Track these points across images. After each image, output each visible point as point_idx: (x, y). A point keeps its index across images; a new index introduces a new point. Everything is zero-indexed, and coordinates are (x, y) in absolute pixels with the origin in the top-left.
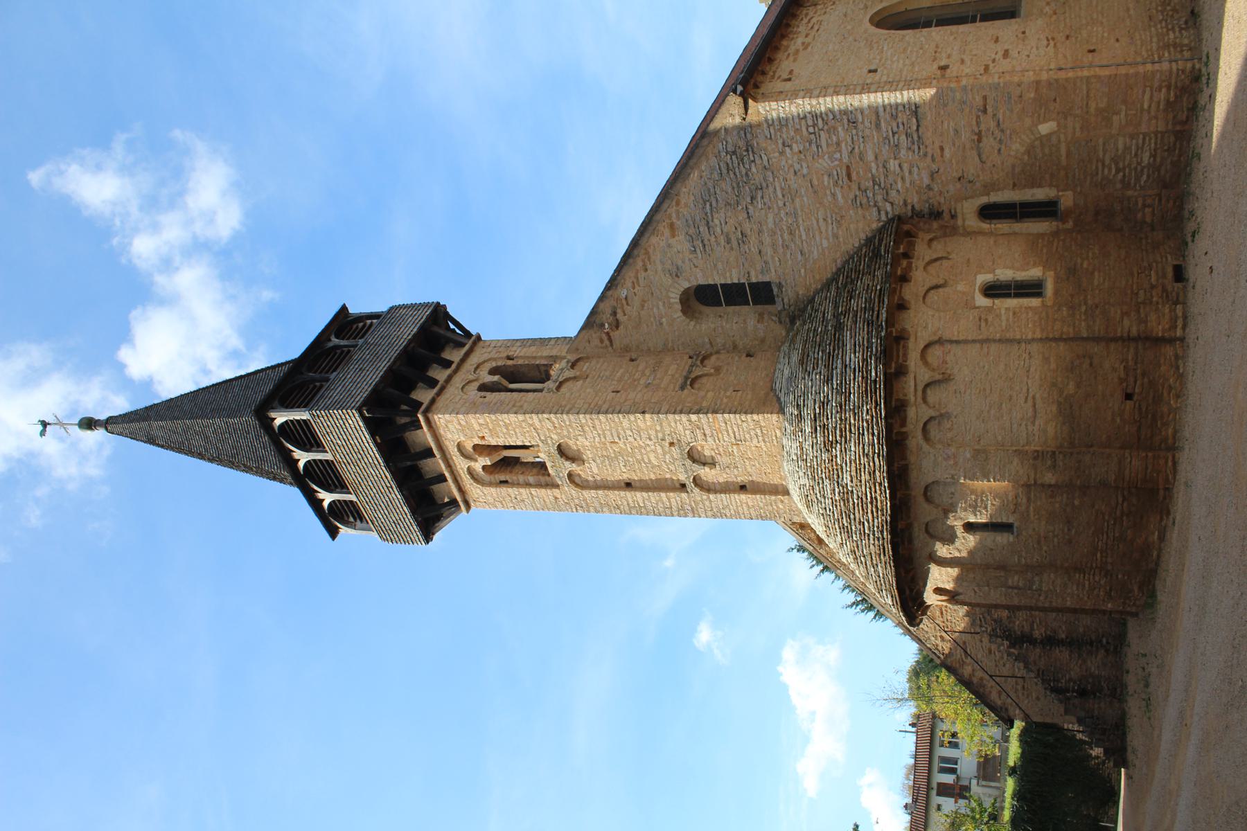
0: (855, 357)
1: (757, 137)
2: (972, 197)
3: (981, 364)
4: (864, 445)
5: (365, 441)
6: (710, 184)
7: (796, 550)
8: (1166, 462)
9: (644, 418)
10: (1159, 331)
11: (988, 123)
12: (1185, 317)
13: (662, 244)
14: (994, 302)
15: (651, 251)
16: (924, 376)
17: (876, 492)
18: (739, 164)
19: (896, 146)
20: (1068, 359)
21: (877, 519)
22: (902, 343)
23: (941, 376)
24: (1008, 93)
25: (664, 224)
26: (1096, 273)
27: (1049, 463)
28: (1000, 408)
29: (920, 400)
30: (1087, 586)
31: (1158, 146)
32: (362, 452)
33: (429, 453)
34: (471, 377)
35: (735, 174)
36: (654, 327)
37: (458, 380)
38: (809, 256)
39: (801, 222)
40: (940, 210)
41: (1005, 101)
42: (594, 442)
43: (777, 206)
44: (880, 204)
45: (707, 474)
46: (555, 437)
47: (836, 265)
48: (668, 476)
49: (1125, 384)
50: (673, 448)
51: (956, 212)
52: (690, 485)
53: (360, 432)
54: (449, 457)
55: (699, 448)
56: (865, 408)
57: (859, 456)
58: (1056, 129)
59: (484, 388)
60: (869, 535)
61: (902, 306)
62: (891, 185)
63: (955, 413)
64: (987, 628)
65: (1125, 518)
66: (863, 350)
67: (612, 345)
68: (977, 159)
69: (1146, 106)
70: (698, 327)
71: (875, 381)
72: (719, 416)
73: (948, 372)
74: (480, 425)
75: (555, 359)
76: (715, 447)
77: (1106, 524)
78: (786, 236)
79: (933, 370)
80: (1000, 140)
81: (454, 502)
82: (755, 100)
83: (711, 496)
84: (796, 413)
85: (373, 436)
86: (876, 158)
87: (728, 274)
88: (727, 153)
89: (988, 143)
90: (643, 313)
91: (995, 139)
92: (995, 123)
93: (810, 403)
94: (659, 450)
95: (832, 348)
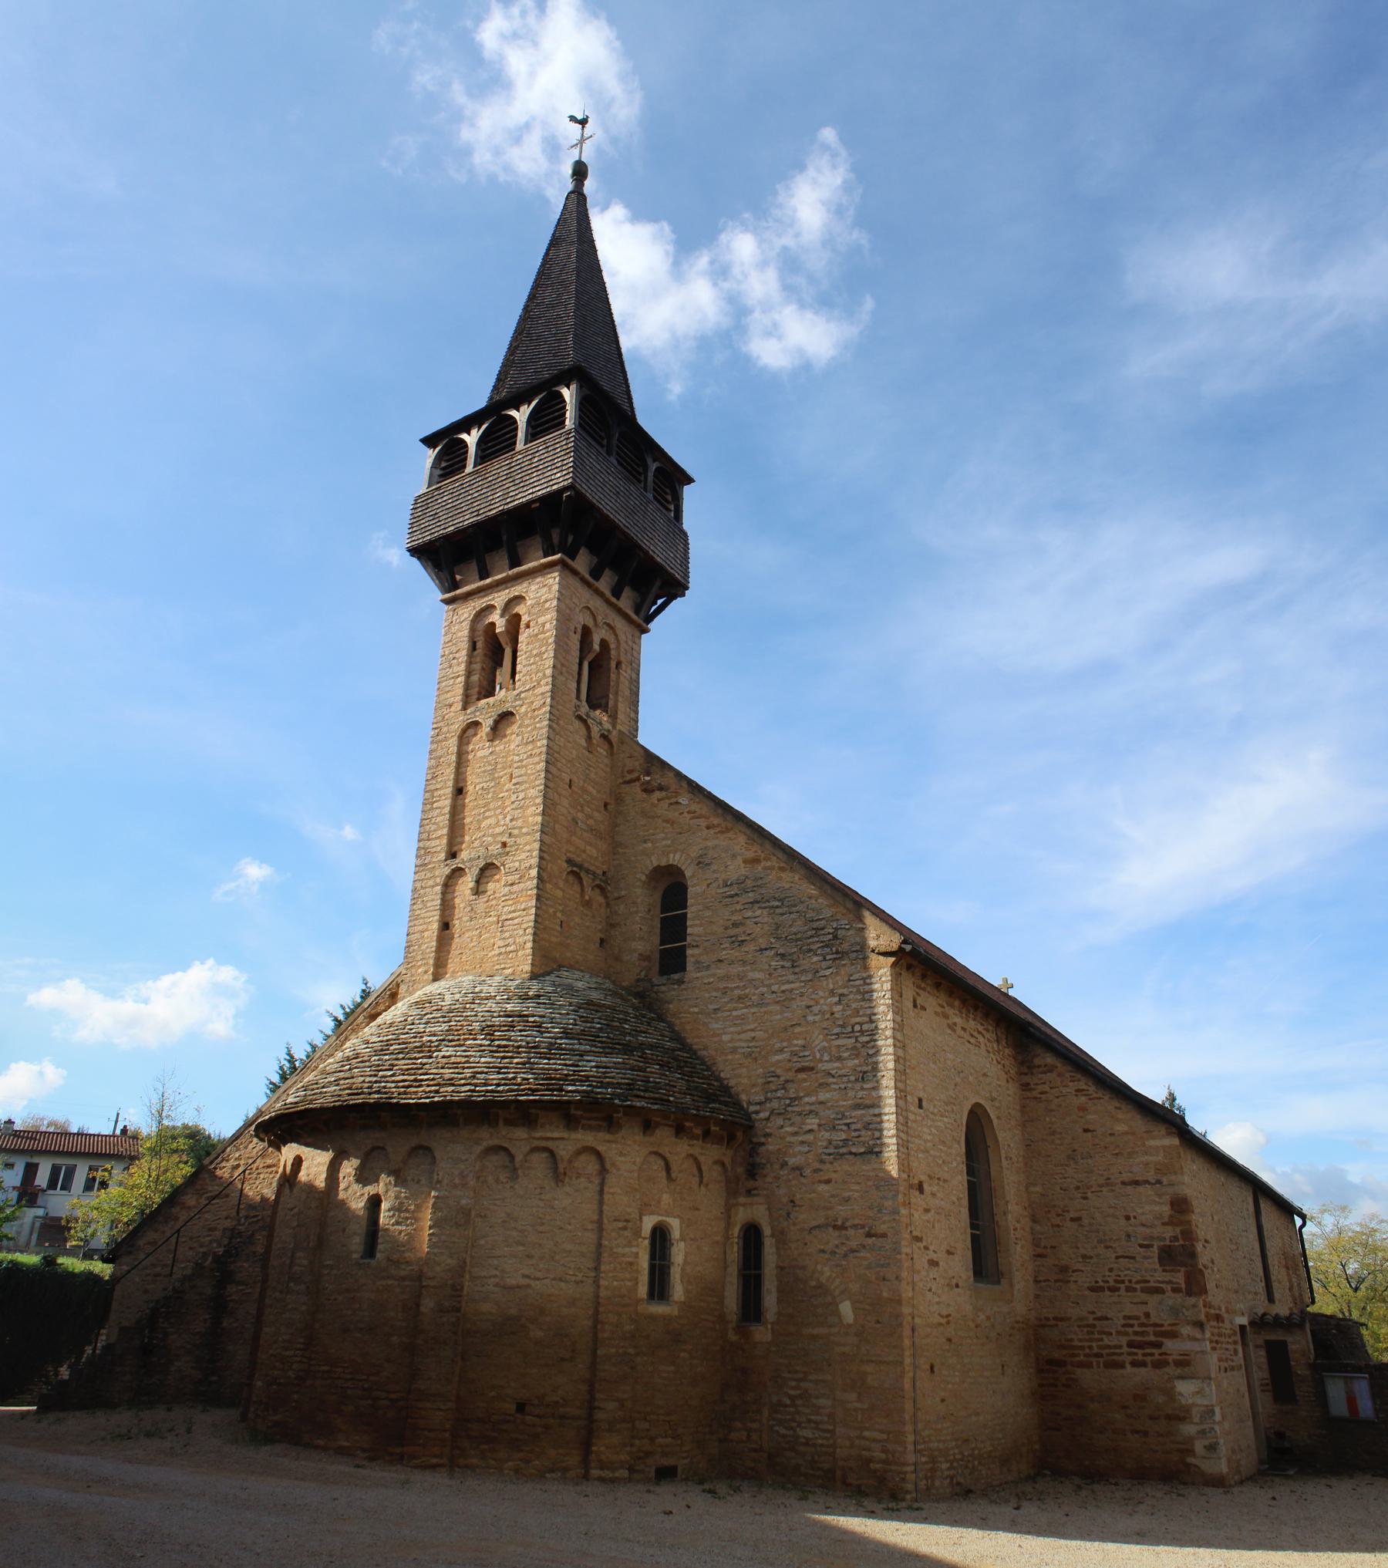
0: (592, 1067)
1: (852, 964)
2: (770, 1215)
3: (573, 1221)
4: (486, 1073)
5: (534, 490)
6: (800, 907)
7: (364, 987)
8: (435, 1456)
9: (538, 814)
10: (599, 1447)
11: (855, 1238)
12: (613, 1481)
13: (737, 848)
14: (645, 1238)
15: (730, 835)
16: (564, 1149)
17: (428, 1086)
18: (822, 942)
19: (834, 1127)
20: (572, 1330)
21: (395, 1086)
22: (604, 1124)
23: (562, 1171)
24: (889, 1264)
25: (760, 852)
26: (672, 1368)
27: (447, 1304)
28: (518, 1243)
29: (536, 1143)
30: (288, 1353)
31: (819, 1449)
32: (522, 485)
33: (515, 562)
34: (599, 618)
35: (811, 937)
36: (641, 833)
37: (597, 603)
38: (712, 1018)
39: (752, 1010)
40: (757, 1177)
41: (880, 1260)
42: (514, 755)
43: (773, 984)
44: (768, 1105)
45: (466, 884)
46: (523, 709)
47: (700, 1050)
48: (467, 838)
49: (536, 1402)
50: (499, 846)
51: (754, 1195)
52: (454, 864)
53: (546, 485)
54: (509, 585)
55: (497, 877)
56: (530, 1076)
57: (474, 1067)
58: (845, 1322)
59: (586, 633)
60: (376, 1076)
61: (648, 1126)
62: (790, 1119)
63: (516, 1186)
64: (243, 1225)
65: (370, 1402)
66: (599, 1077)
67: (625, 783)
68: (814, 1223)
69: (866, 1433)
70: (638, 884)
71: (562, 1090)
72: (534, 902)
73: (567, 1180)
74: (543, 625)
75: (614, 717)
76: (497, 895)
77: (364, 1377)
78: (737, 992)
79: (570, 1162)
80: (835, 1252)
81: (455, 586)
82: (894, 965)
83: (439, 887)
84: (530, 993)
85: (542, 499)
86: (821, 1103)
87: (698, 922)
88: (836, 929)
89: (832, 1238)
90: (660, 820)
91: (837, 1246)
92: (855, 1247)
93: (541, 1011)
94: (498, 830)
95: (604, 1039)
